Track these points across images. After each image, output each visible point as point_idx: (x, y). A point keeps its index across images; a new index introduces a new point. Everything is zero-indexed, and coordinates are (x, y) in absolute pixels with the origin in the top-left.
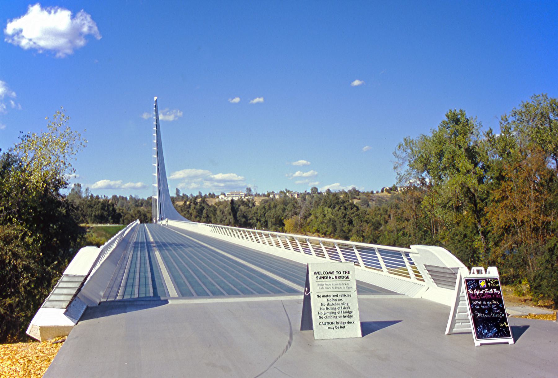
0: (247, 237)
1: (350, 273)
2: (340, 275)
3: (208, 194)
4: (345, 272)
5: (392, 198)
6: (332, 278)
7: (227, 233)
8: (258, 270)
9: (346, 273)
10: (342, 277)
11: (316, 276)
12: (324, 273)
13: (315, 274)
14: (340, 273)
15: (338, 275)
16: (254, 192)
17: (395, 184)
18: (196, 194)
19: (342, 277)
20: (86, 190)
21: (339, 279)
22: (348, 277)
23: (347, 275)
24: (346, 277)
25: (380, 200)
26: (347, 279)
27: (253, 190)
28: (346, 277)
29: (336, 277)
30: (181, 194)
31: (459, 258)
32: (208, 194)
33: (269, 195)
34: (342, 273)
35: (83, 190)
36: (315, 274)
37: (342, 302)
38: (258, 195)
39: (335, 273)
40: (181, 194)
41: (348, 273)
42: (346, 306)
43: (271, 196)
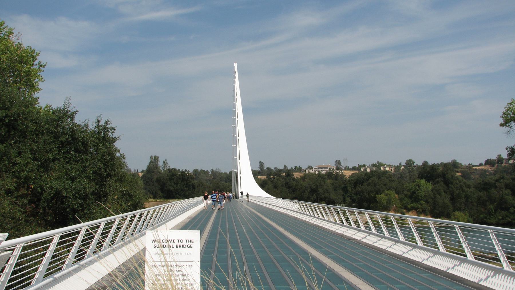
0: (326, 213)
1: (194, 241)
2: (182, 244)
3: (293, 168)
4: (188, 241)
5: (496, 172)
6: (172, 247)
7: (308, 209)
8: (322, 260)
9: (189, 241)
10: (183, 246)
11: (154, 243)
12: (164, 241)
13: (153, 242)
14: (182, 241)
15: (180, 243)
16: (343, 165)
17: (367, 166)
18: (281, 167)
19: (183, 246)
20: (164, 162)
21: (180, 248)
22: (191, 246)
23: (190, 243)
24: (188, 246)
25: (483, 173)
26: (190, 248)
27: (342, 164)
28: (188, 246)
29: (177, 246)
30: (265, 168)
31: (99, 219)
32: (293, 168)
33: (360, 167)
34: (185, 241)
35: (160, 164)
36: (153, 242)
37: (181, 273)
38: (347, 169)
39: (176, 241)
40: (265, 168)
41: (192, 241)
42: (185, 278)
43: (362, 169)
